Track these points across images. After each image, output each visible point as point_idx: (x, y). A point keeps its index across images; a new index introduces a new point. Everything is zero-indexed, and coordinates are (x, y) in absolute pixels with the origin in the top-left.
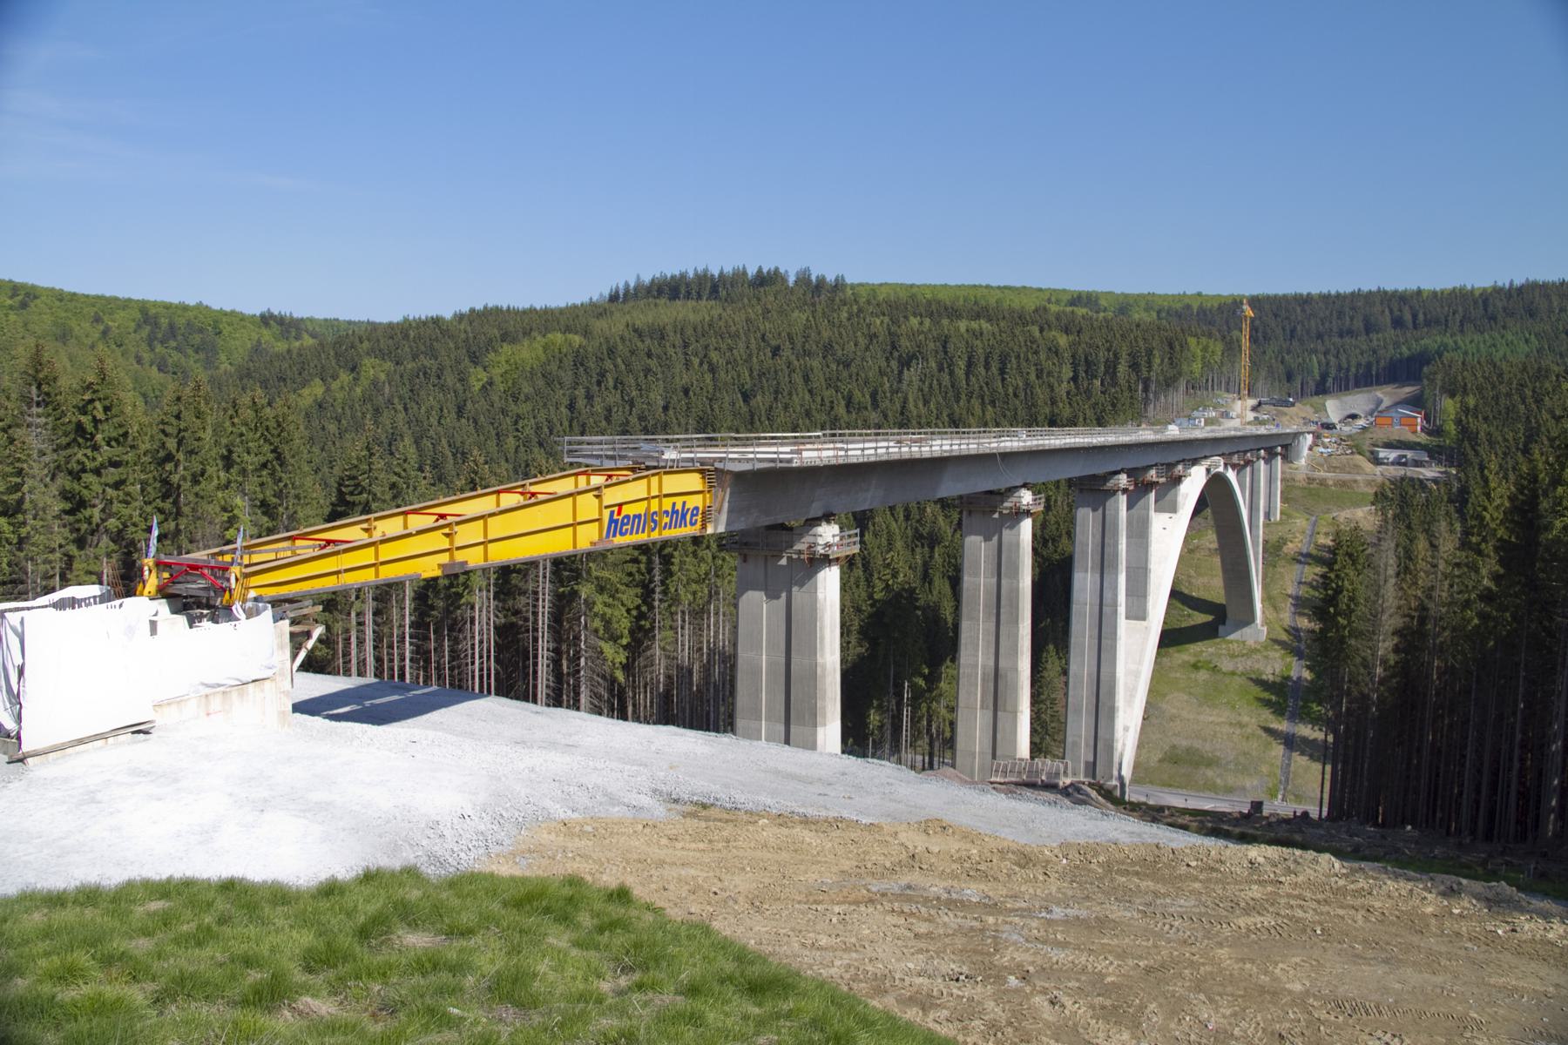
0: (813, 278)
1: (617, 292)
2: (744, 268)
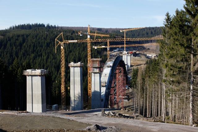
0: (50, 26)
1: (11, 27)
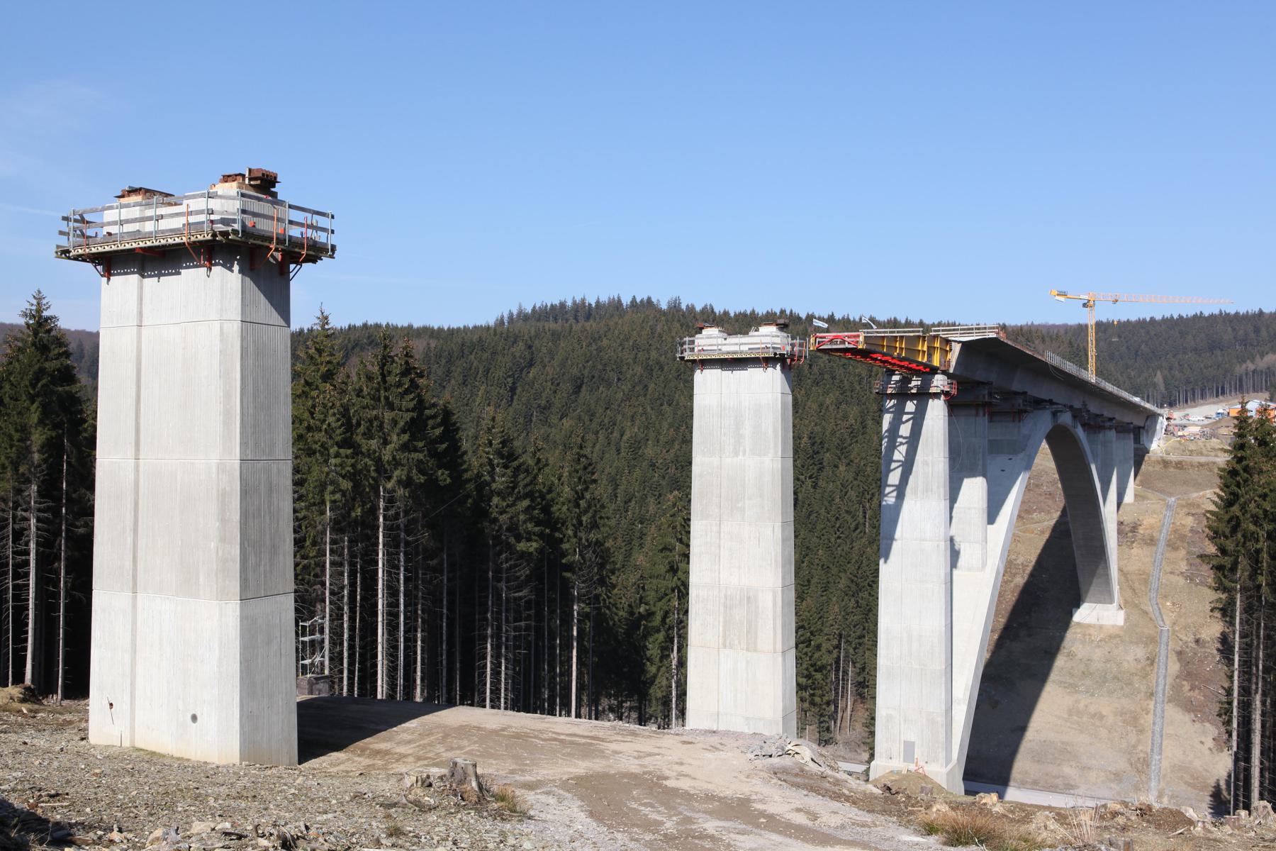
0: (684, 307)
2: (619, 298)
